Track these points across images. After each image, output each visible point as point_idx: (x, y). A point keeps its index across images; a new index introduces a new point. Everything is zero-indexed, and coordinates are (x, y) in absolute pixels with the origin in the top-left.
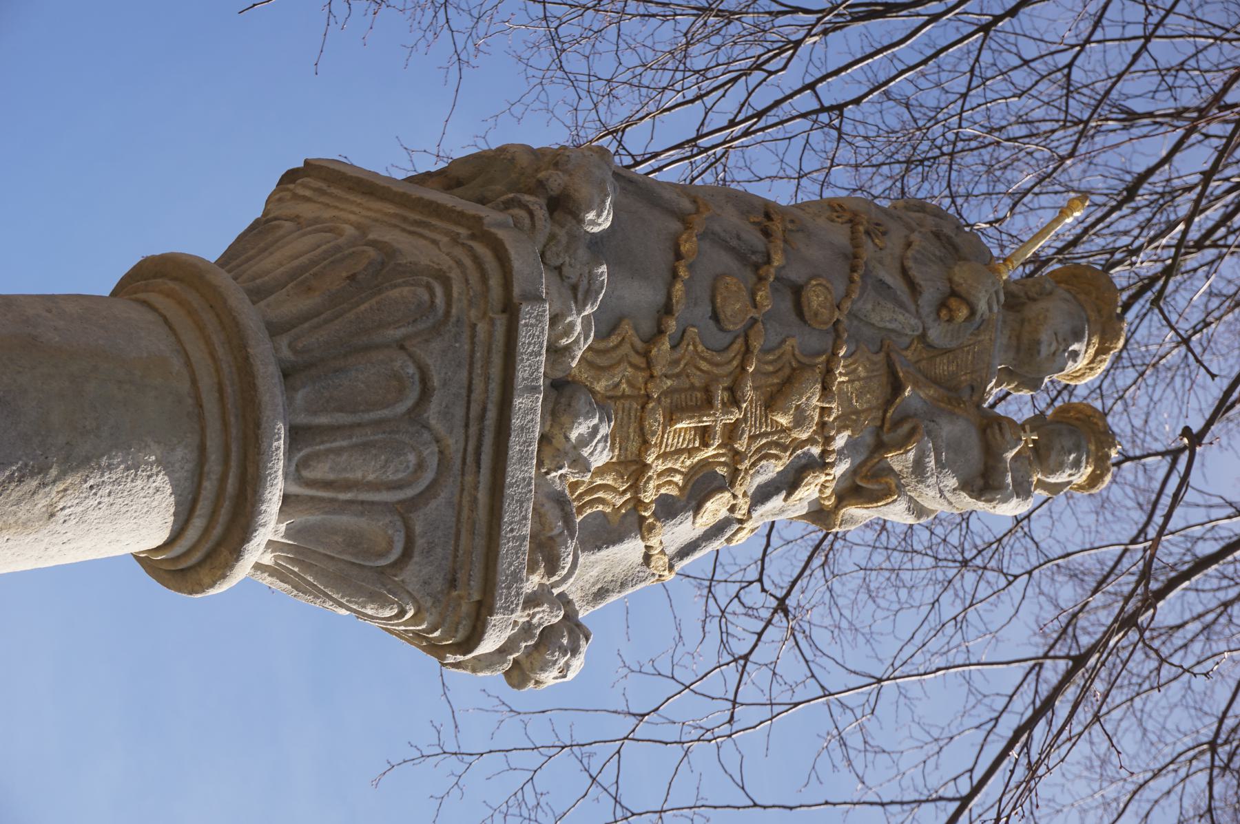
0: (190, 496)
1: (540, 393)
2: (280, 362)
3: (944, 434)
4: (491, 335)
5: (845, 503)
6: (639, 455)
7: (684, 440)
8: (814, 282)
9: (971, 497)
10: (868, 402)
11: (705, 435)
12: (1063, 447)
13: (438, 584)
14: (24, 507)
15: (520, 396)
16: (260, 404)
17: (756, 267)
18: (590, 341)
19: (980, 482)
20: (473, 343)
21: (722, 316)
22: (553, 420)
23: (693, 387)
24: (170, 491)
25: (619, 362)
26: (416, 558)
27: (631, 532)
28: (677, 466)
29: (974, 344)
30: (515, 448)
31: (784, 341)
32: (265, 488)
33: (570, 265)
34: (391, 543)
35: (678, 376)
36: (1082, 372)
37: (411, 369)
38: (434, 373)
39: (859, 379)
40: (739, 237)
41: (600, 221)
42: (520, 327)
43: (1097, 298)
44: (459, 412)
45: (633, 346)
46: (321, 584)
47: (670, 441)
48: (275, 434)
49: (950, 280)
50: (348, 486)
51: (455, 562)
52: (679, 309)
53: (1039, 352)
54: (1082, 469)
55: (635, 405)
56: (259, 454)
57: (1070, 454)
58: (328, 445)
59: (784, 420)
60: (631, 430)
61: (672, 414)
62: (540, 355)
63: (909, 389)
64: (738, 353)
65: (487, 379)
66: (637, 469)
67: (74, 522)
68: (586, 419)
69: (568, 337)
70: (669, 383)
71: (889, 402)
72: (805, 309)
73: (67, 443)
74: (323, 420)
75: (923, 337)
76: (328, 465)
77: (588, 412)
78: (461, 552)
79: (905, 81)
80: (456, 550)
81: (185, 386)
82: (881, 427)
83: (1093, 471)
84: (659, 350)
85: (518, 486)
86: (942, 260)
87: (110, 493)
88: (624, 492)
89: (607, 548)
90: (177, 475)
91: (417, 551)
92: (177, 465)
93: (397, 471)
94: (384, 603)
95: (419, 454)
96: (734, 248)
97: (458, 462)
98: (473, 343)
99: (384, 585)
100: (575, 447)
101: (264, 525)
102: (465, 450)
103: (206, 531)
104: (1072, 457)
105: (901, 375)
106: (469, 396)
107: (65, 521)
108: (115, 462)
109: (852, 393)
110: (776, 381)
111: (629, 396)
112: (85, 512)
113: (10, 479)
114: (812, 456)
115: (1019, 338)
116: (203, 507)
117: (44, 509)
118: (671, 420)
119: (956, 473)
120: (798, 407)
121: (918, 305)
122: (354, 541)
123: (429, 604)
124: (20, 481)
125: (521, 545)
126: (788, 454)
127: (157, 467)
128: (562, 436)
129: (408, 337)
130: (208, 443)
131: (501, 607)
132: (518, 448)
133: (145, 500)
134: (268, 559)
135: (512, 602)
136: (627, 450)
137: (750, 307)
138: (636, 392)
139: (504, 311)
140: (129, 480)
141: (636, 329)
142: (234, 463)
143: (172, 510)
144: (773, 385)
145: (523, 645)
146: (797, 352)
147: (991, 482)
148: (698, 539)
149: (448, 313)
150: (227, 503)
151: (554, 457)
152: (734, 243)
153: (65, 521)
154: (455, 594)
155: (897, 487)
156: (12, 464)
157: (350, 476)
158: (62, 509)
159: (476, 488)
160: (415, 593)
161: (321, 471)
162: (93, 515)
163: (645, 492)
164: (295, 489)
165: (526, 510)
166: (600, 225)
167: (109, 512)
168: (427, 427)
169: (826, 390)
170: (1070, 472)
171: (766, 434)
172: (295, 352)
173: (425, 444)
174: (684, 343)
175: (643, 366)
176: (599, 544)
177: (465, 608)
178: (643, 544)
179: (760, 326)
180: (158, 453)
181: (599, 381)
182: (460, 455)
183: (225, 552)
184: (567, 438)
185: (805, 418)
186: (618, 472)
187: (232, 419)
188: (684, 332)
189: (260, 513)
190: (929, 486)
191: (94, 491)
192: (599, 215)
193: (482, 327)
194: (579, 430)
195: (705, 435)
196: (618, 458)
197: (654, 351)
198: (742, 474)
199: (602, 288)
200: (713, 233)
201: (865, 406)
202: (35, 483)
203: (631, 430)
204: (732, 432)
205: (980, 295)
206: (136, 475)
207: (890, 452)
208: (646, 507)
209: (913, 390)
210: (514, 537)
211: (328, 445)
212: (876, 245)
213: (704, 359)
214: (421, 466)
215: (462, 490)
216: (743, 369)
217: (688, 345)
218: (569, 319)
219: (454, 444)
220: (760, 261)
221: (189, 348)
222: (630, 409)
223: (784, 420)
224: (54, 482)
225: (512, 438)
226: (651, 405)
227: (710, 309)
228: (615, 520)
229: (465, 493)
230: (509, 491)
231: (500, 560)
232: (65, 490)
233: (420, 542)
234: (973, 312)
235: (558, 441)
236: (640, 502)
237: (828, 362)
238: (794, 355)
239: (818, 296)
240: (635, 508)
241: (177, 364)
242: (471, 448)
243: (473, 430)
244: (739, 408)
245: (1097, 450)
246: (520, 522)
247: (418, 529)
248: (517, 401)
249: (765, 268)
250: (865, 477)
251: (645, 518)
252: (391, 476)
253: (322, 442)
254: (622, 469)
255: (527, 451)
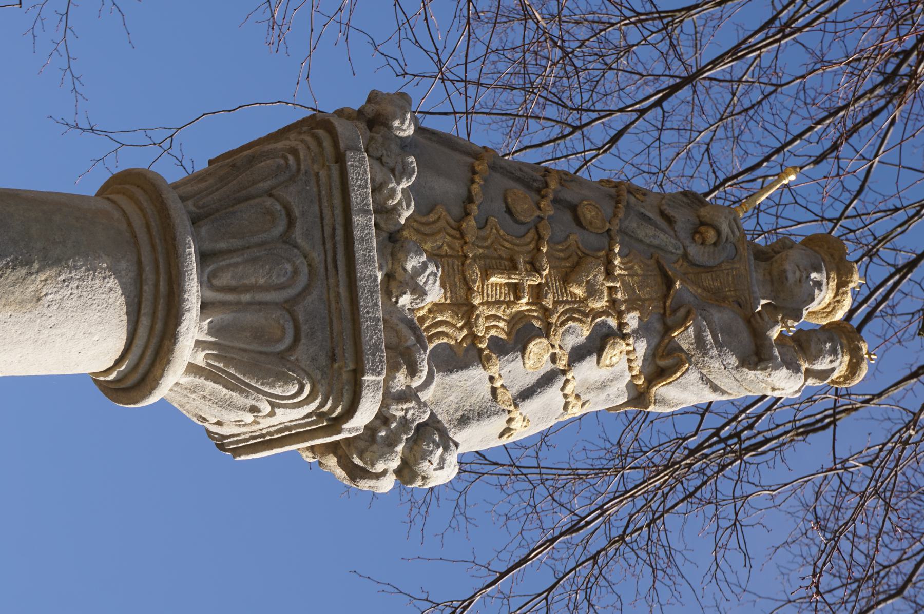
0: (136, 300)
1: (371, 215)
2: (189, 213)
3: (715, 319)
4: (329, 177)
5: (654, 383)
6: (467, 299)
7: (501, 293)
8: (585, 202)
9: (750, 369)
10: (649, 293)
11: (516, 290)
12: (819, 339)
13: (323, 360)
14: (18, 290)
15: (356, 215)
16: (174, 225)
17: (538, 191)
18: (411, 212)
19: (755, 359)
20: (319, 186)
21: (514, 210)
22: (393, 259)
23: (500, 257)
24: (120, 292)
25: (439, 232)
26: (303, 341)
27: (474, 362)
28: (500, 314)
29: (732, 269)
30: (359, 253)
31: (568, 236)
32: (185, 281)
33: (388, 156)
34: (284, 330)
35: (487, 248)
36: (832, 306)
37: (278, 207)
38: (294, 207)
39: (637, 275)
40: (521, 170)
41: (404, 127)
42: (348, 167)
43: (829, 248)
44: (317, 234)
45: (448, 223)
46: (240, 373)
47: (490, 292)
48: (187, 244)
49: (698, 217)
50: (247, 289)
51: (332, 342)
52: (478, 199)
53: (787, 278)
54: (840, 356)
55: (457, 262)
56: (177, 258)
57: (826, 343)
58: (228, 261)
59: (579, 291)
60: (457, 279)
61: (486, 271)
62: (367, 188)
63: (678, 283)
64: (532, 240)
65: (332, 207)
66: (468, 311)
67: (55, 307)
68: (416, 255)
69: (393, 199)
70: (481, 251)
71: (666, 297)
72: (582, 218)
73: (44, 248)
74: (223, 245)
75: (685, 256)
76: (230, 274)
77: (417, 251)
78: (335, 334)
79: (836, 475)
80: (332, 333)
81: (124, 226)
82: (664, 314)
83: (850, 360)
84: (467, 224)
85: (367, 280)
86: (690, 206)
87: (78, 287)
88: (461, 329)
89: (457, 371)
90: (124, 280)
91: (303, 335)
92: (123, 273)
93: (279, 276)
94: (287, 380)
95: (293, 264)
96: (520, 178)
97: (322, 270)
98: (319, 186)
99: (284, 365)
100: (412, 278)
101: (189, 311)
102: (326, 261)
103: (152, 328)
104: (828, 345)
105: (670, 273)
106: (322, 223)
107: (49, 306)
108: (79, 264)
109: (633, 285)
110: (567, 264)
111: (451, 256)
112: (62, 299)
113: (7, 266)
114: (610, 327)
115: (770, 274)
116: (146, 309)
117: (33, 294)
118: (486, 276)
119: (734, 352)
120: (588, 282)
121: (675, 231)
122: (258, 334)
123: (319, 377)
124: (14, 269)
125: (376, 324)
126: (590, 319)
127: (109, 271)
128: (400, 269)
129: (272, 188)
130: (143, 259)
131: (369, 369)
132: (362, 253)
133: (104, 296)
134: (200, 359)
135: (378, 366)
136: (456, 294)
137: (535, 208)
138: (456, 253)
139: (336, 162)
140: (90, 278)
141: (448, 211)
142: (162, 270)
143: (125, 310)
144: (567, 267)
145: (405, 437)
146: (580, 246)
147: (763, 357)
148: (534, 386)
149: (299, 170)
150: (162, 301)
151: (399, 287)
152: (518, 174)
153: (49, 306)
154: (336, 366)
155: (687, 358)
156: (6, 256)
157: (246, 281)
158: (46, 295)
159: (338, 286)
160: (307, 369)
161: (225, 279)
162: (68, 303)
163: (477, 326)
164: (211, 295)
165: (376, 299)
166: (405, 130)
167: (78, 302)
168: (296, 246)
169: (609, 274)
170: (830, 358)
171: (567, 302)
172: (198, 207)
173: (296, 256)
174: (488, 227)
175: (458, 236)
176: (450, 368)
177: (345, 376)
178: (485, 375)
179: (546, 222)
180: (109, 263)
181: (426, 243)
182: (323, 265)
183: (167, 342)
184: (405, 269)
185: (596, 291)
186: (453, 311)
187: (157, 241)
188: (487, 220)
189: (184, 301)
190: (712, 357)
191: (66, 284)
192: (403, 123)
193: (323, 174)
194: (412, 263)
195: (516, 290)
196: (451, 300)
197: (464, 225)
198: (554, 327)
199: (414, 172)
200: (501, 168)
201: (647, 296)
202: (24, 272)
203: (457, 279)
204: (538, 293)
205: (721, 220)
206: (94, 275)
207: (675, 331)
208: (481, 339)
209: (681, 283)
210: (370, 318)
211: (228, 261)
212: (637, 199)
213: (507, 241)
214: (296, 272)
215: (329, 289)
216: (539, 250)
217: (492, 229)
218: (390, 186)
219: (317, 256)
220: (541, 186)
221: (125, 207)
222: (453, 264)
223: (579, 291)
224: (37, 272)
225: (356, 245)
226: (468, 261)
227: (504, 205)
228: (460, 352)
229: (331, 291)
230: (361, 283)
231: (363, 334)
232: (46, 280)
233: (305, 328)
234: (719, 233)
235: (399, 275)
236: (475, 337)
237: (607, 256)
238: (579, 248)
239: (590, 211)
240: (473, 344)
241: (117, 215)
242: (329, 259)
243: (329, 245)
244: (541, 275)
245: (849, 344)
246: (373, 307)
247: (301, 318)
248: (355, 219)
249: (545, 190)
250: (662, 357)
251: (481, 350)
252: (275, 280)
253: (224, 260)
254: (455, 309)
255: (369, 255)
